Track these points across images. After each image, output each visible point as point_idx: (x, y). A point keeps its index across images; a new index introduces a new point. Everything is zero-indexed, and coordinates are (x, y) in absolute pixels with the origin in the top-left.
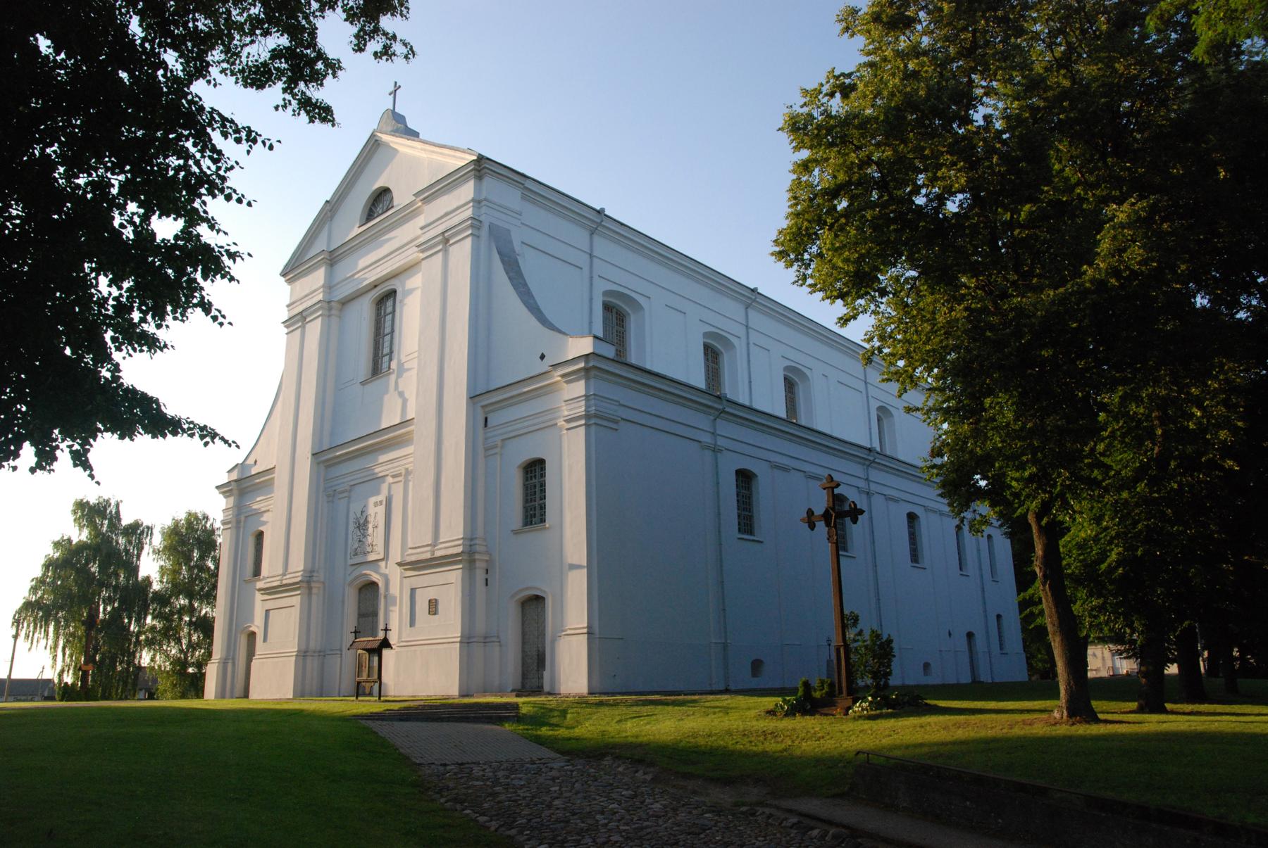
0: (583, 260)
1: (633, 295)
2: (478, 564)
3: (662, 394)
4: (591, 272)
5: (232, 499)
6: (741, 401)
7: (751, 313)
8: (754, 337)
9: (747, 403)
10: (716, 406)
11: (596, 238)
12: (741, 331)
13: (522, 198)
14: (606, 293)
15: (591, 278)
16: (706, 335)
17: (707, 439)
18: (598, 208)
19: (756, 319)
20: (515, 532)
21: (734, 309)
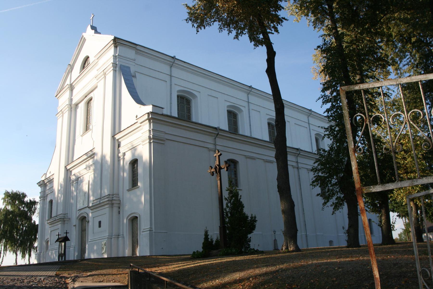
0: (167, 78)
1: (192, 91)
2: (115, 205)
3: (167, 124)
4: (171, 82)
5: (43, 188)
6: (246, 135)
7: (310, 118)
8: (252, 107)
9: (249, 135)
10: (215, 132)
11: (249, 96)
12: (246, 104)
13: (136, 53)
14: (178, 91)
15: (171, 85)
16: (228, 106)
17: (211, 146)
18: (173, 56)
19: (253, 99)
20: (129, 190)
21: (243, 96)
